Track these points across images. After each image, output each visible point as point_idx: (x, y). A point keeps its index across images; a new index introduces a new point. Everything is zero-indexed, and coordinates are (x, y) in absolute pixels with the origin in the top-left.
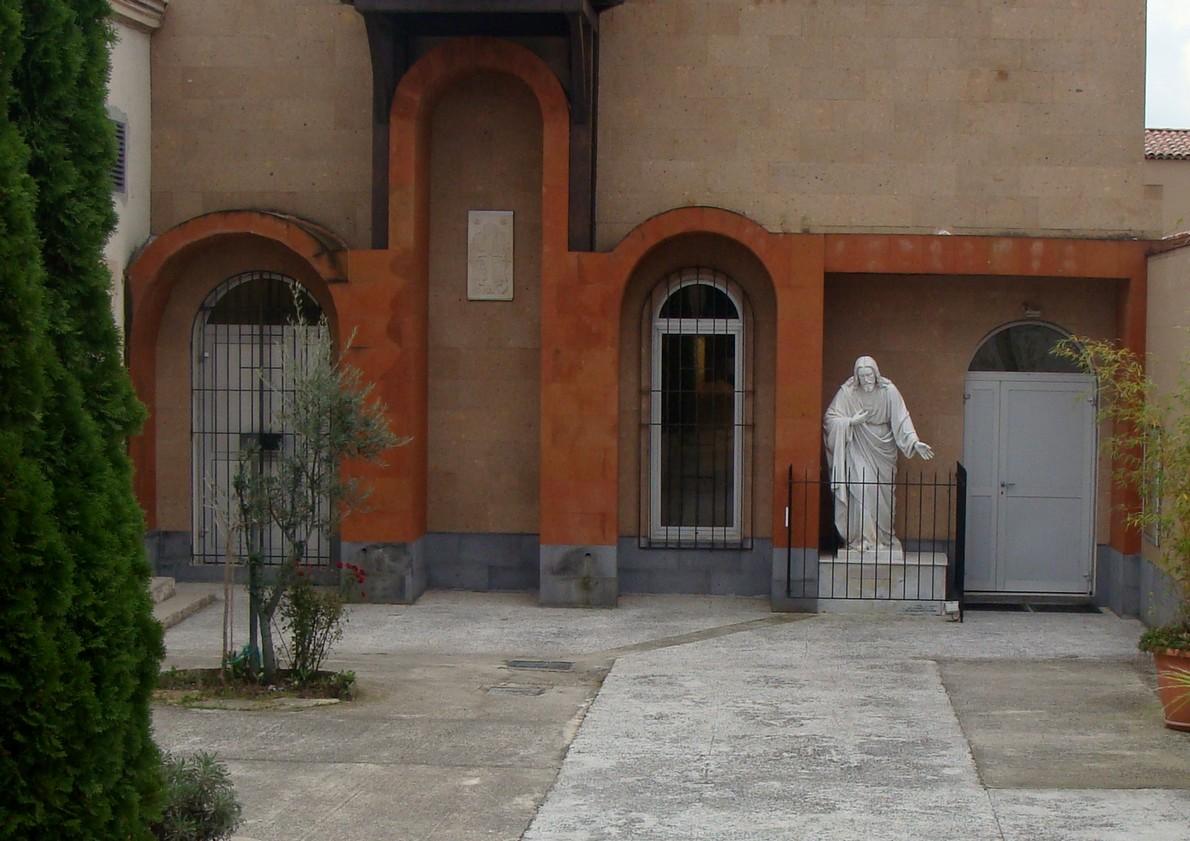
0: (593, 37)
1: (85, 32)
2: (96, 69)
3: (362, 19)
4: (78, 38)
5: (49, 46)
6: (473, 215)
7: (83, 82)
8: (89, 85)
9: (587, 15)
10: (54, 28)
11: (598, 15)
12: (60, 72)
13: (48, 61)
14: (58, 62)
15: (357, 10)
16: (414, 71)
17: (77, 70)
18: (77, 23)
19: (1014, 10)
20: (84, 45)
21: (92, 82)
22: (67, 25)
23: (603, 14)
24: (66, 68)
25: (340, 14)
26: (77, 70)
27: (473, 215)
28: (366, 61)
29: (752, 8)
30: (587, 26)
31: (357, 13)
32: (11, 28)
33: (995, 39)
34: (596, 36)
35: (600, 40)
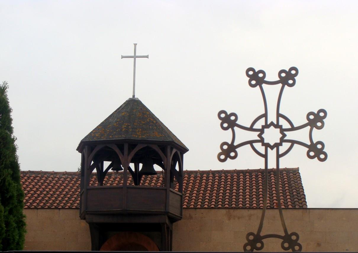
0: (170, 233)
1: (19, 230)
2: (21, 240)
3: (88, 225)
4: (17, 231)
5: (10, 234)
6: (104, 162)
7: (18, 244)
8: (20, 245)
9: (168, 224)
10: (11, 229)
11: (172, 224)
12: (12, 241)
13: (9, 238)
14: (12, 238)
15: (87, 222)
16: (106, 243)
17: (16, 240)
18: (17, 227)
19: (322, 221)
20: (18, 233)
21: (20, 244)
22: (14, 228)
23: (174, 224)
24: (14, 240)
25: (80, 223)
26: (16, 240)
27: (104, 162)
28: (89, 240)
29: (227, 221)
30: (168, 228)
31: (86, 223)
32: (3, 229)
33: (316, 232)
34: (171, 232)
35: (173, 233)
